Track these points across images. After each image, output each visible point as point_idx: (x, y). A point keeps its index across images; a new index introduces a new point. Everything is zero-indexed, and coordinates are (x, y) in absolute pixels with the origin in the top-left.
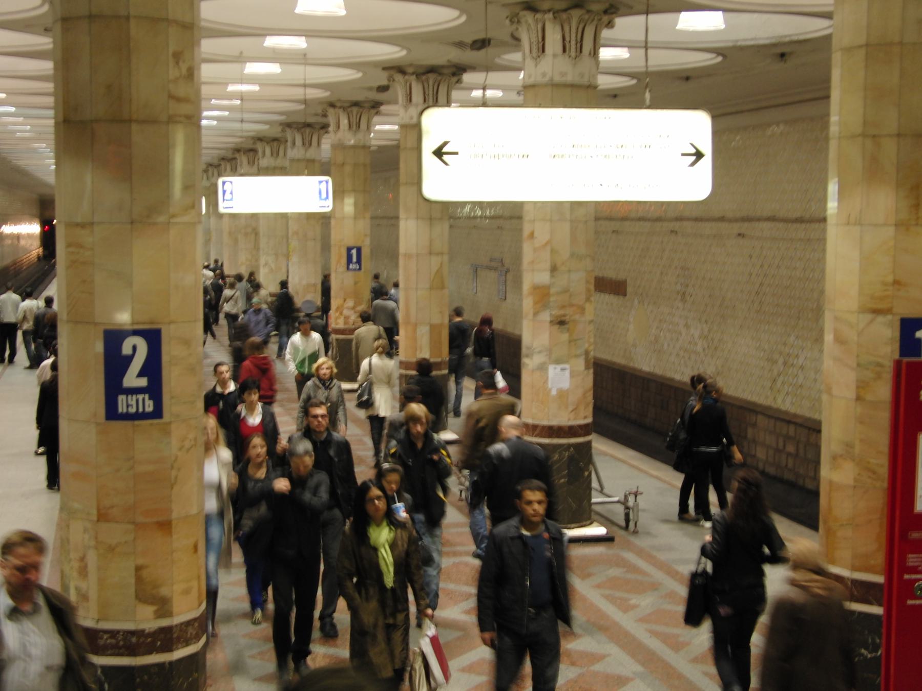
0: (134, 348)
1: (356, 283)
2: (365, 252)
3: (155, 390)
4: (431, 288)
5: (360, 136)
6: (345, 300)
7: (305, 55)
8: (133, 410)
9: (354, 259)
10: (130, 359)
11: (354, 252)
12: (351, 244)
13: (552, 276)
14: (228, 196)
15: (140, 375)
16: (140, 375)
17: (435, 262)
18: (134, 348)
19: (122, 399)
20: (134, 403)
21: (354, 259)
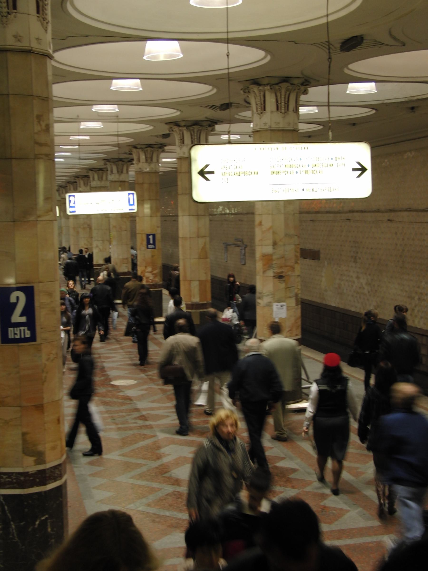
0: (18, 298)
1: (153, 256)
2: (158, 237)
3: (31, 324)
4: (200, 258)
5: (153, 165)
6: (146, 267)
7: (117, 116)
8: (18, 337)
9: (151, 242)
10: (15, 305)
11: (151, 237)
12: (148, 233)
13: (274, 248)
14: (72, 204)
15: (22, 315)
16: (22, 315)
17: (201, 241)
18: (18, 298)
19: (11, 329)
20: (18, 332)
21: (151, 242)
